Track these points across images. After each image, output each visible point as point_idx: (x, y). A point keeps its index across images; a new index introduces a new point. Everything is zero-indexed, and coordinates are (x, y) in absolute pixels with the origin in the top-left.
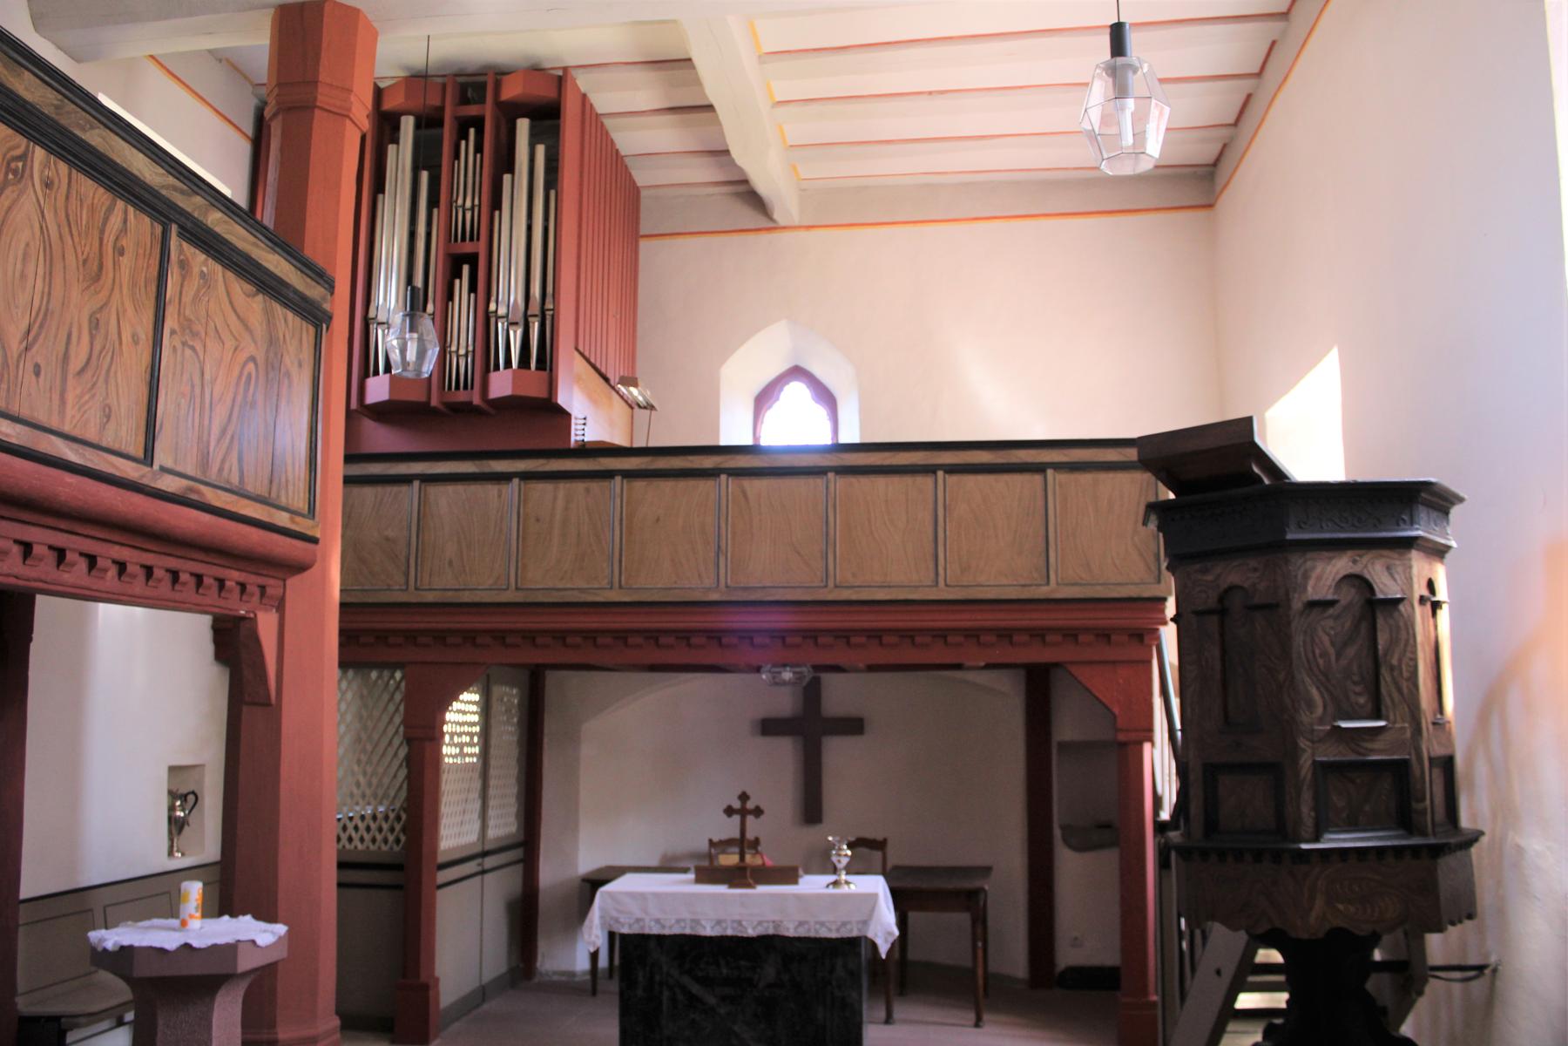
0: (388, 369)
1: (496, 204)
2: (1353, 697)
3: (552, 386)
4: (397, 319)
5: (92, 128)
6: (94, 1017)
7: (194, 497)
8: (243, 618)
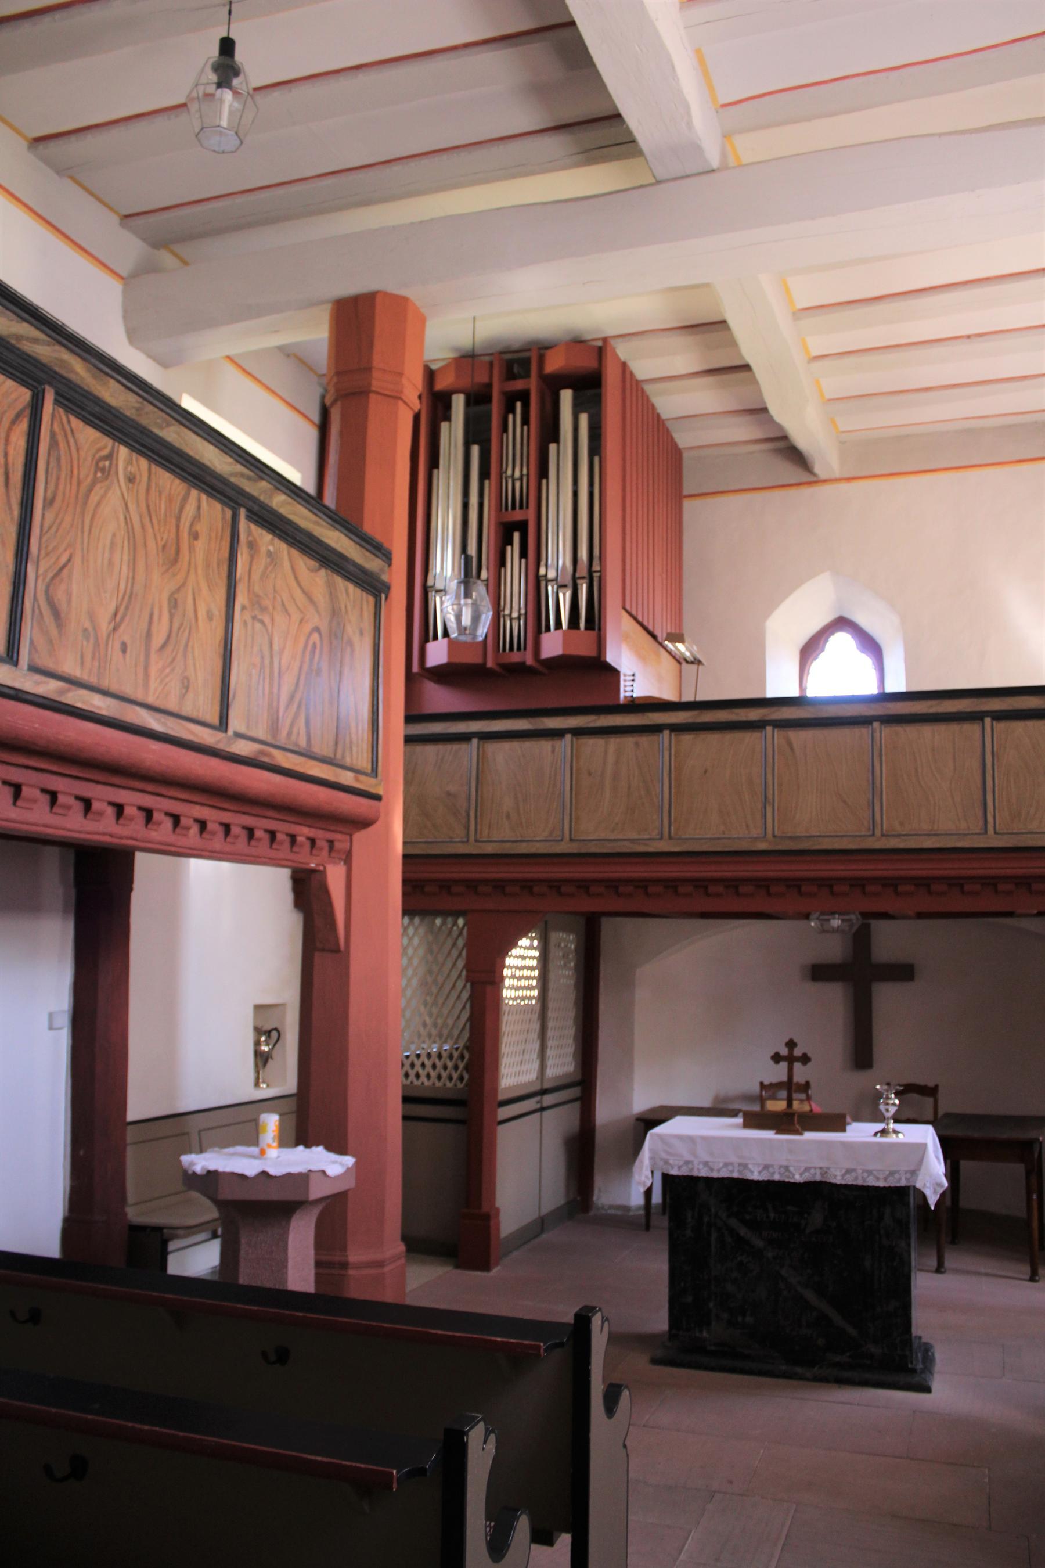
0: (446, 634)
1: (543, 472)
3: (600, 644)
4: (453, 585)
5: (168, 425)
6: (191, 1230)
7: (265, 759)
8: (314, 871)
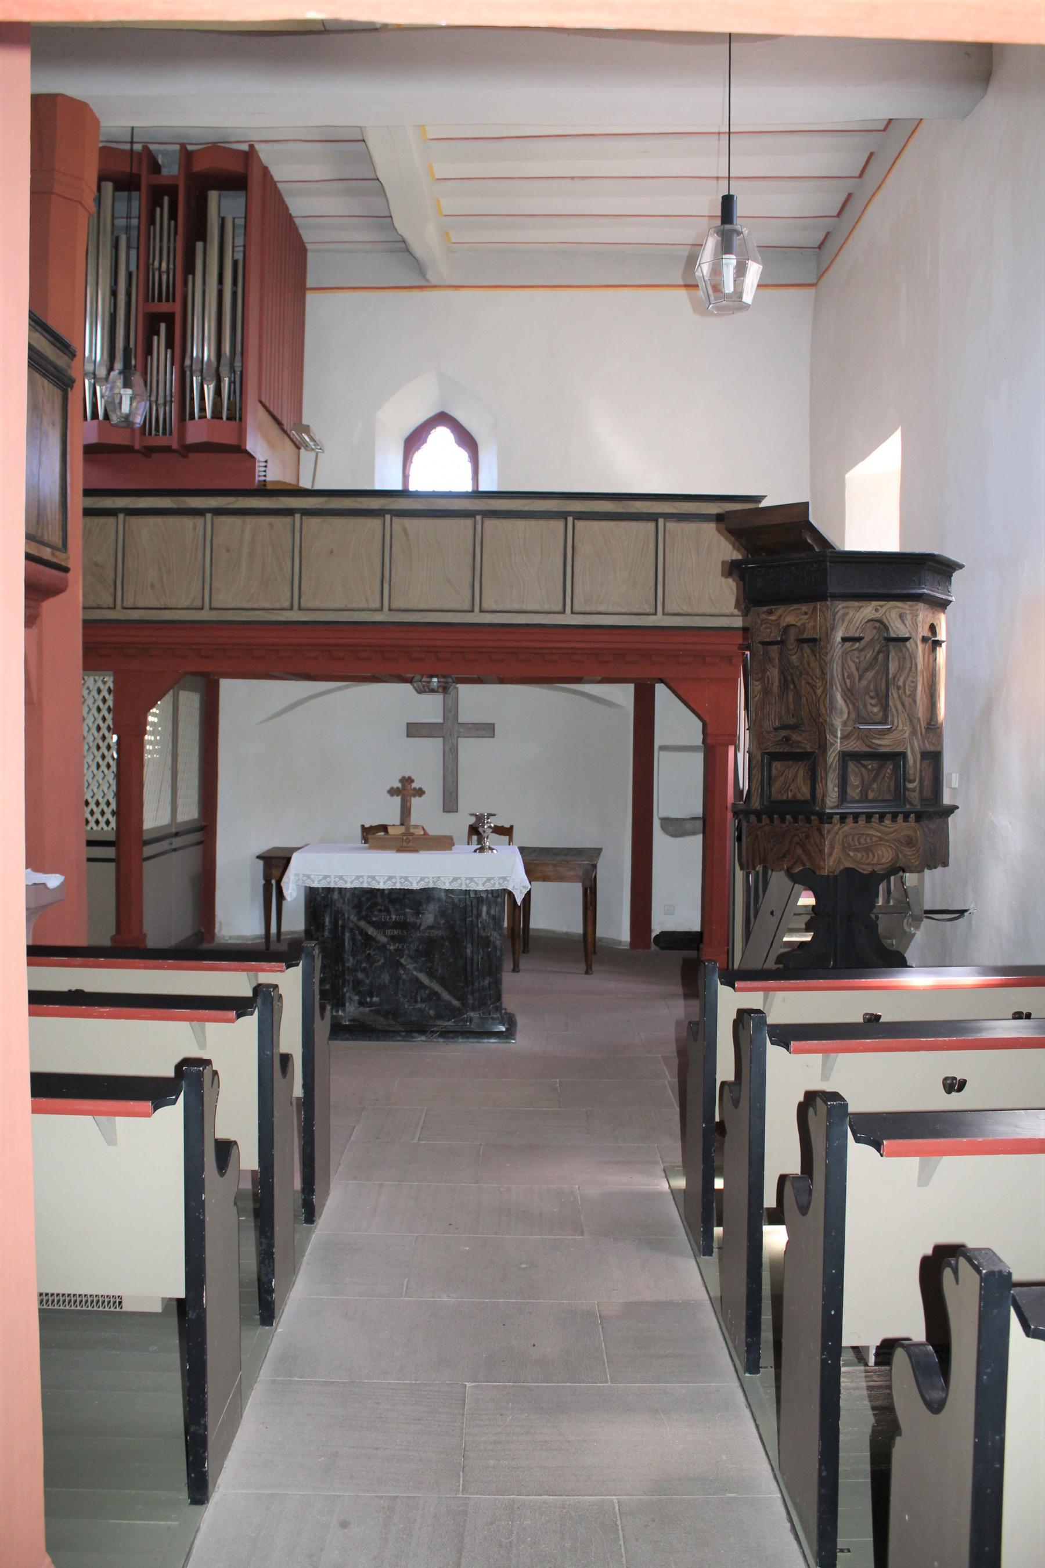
2: (869, 707)
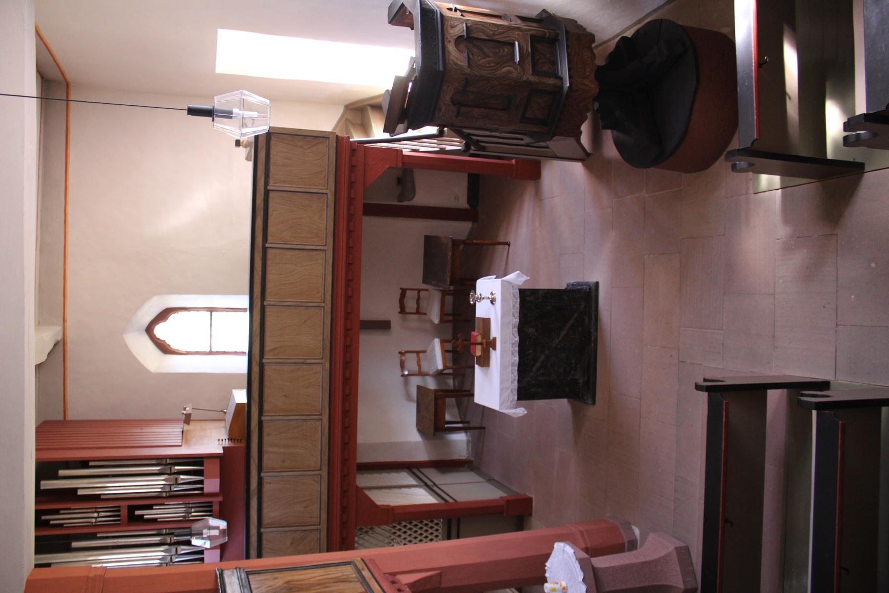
1: (97, 498)
